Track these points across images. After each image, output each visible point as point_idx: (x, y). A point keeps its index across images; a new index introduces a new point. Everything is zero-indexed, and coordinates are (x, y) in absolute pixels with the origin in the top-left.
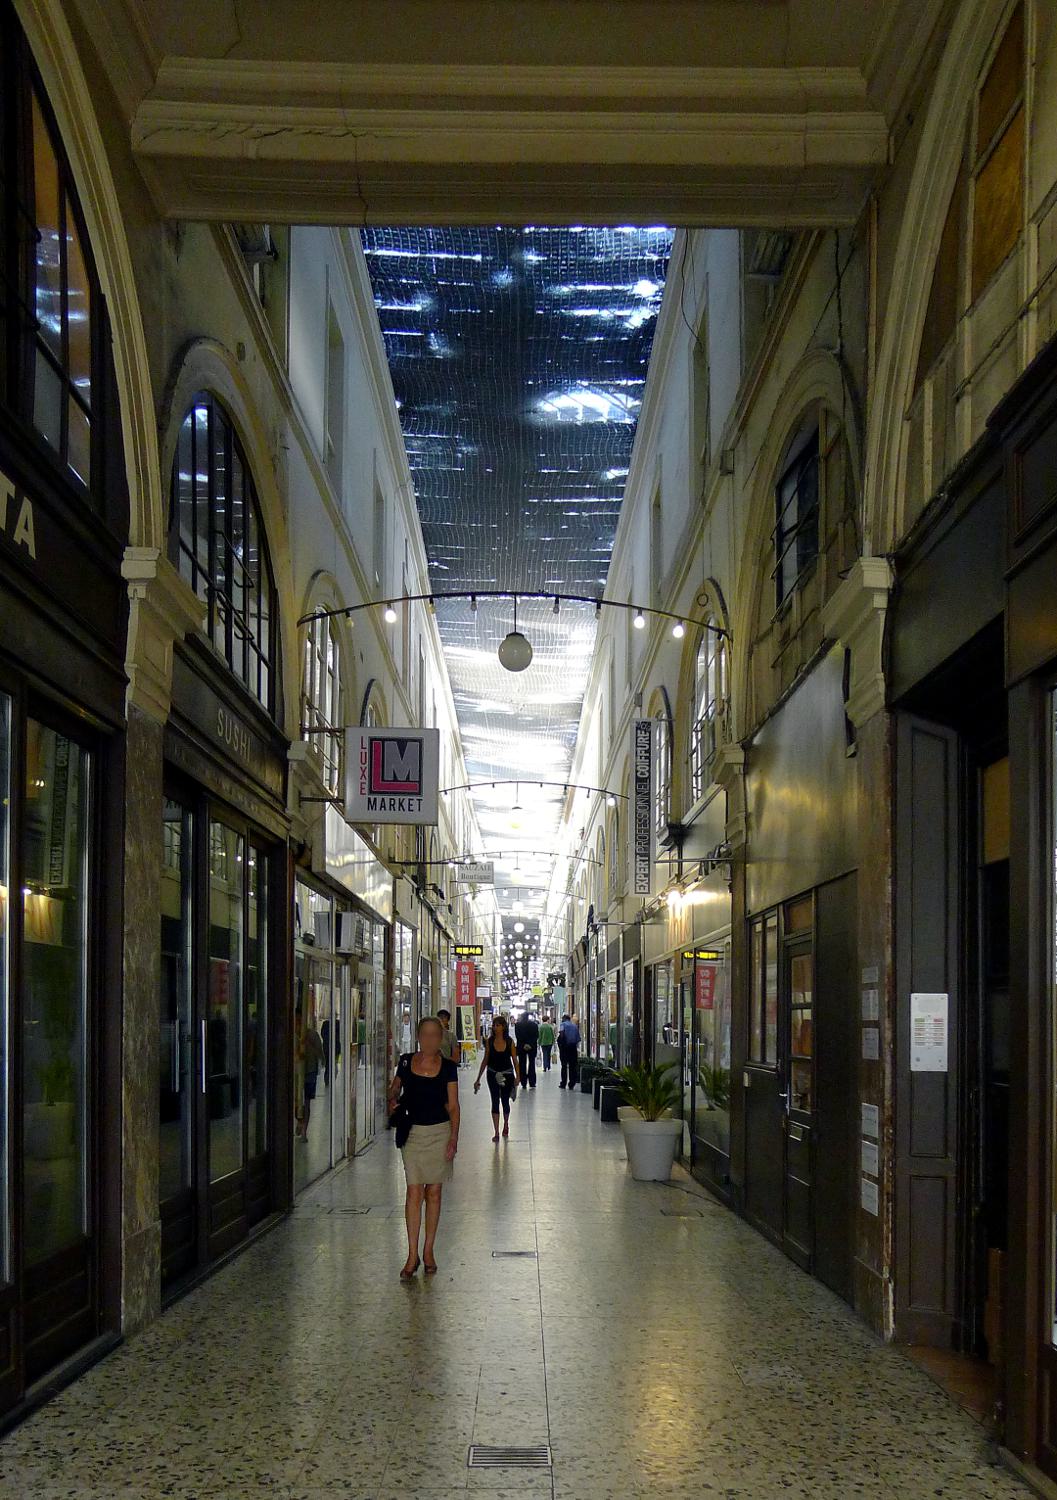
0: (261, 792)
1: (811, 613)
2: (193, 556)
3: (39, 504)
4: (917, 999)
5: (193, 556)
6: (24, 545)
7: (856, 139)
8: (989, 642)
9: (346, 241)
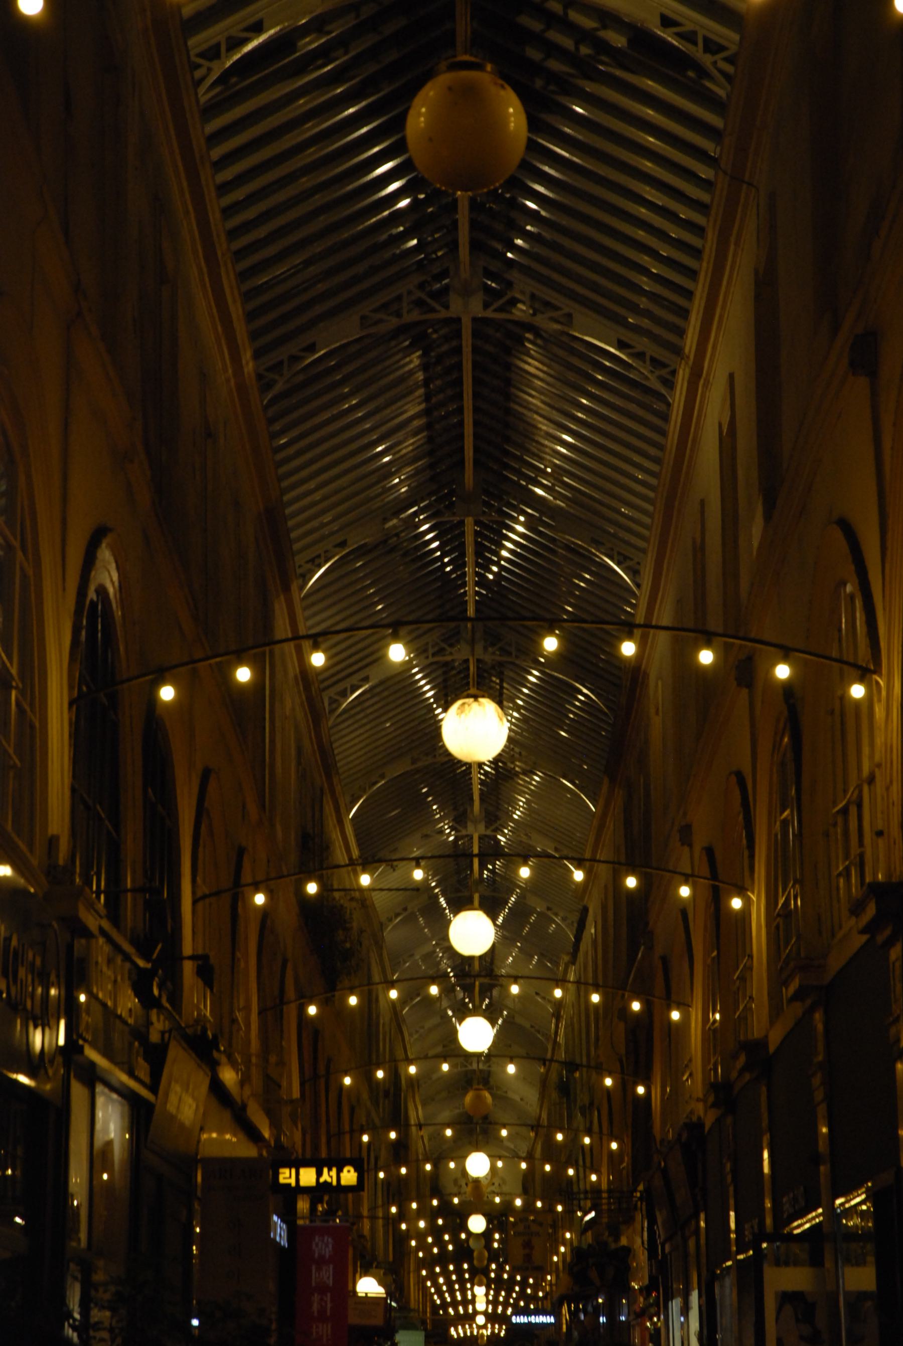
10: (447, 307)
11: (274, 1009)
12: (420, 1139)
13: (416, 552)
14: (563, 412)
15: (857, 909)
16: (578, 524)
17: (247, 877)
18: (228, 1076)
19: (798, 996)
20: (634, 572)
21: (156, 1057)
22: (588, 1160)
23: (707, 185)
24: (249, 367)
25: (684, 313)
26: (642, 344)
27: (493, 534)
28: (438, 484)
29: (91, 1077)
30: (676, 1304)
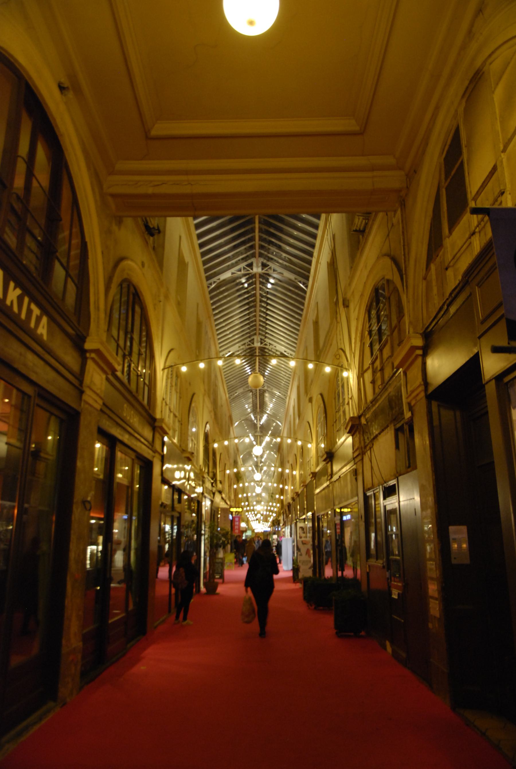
0: (142, 440)
1: (387, 360)
2: (117, 341)
3: (51, 319)
4: (452, 528)
5: (117, 341)
6: (42, 335)
7: (393, 180)
8: (473, 365)
9: (187, 222)
10: (252, 269)
11: (230, 486)
12: (251, 504)
13: (251, 420)
14: (271, 401)
15: (310, 475)
16: (273, 417)
17: (226, 468)
18: (224, 496)
19: (303, 486)
20: (282, 424)
21: (214, 494)
22: (276, 507)
23: (290, 372)
24: (227, 396)
25: (288, 389)
26: (282, 392)
27: (261, 418)
28: (254, 411)
29: (205, 497)
30: (287, 528)
